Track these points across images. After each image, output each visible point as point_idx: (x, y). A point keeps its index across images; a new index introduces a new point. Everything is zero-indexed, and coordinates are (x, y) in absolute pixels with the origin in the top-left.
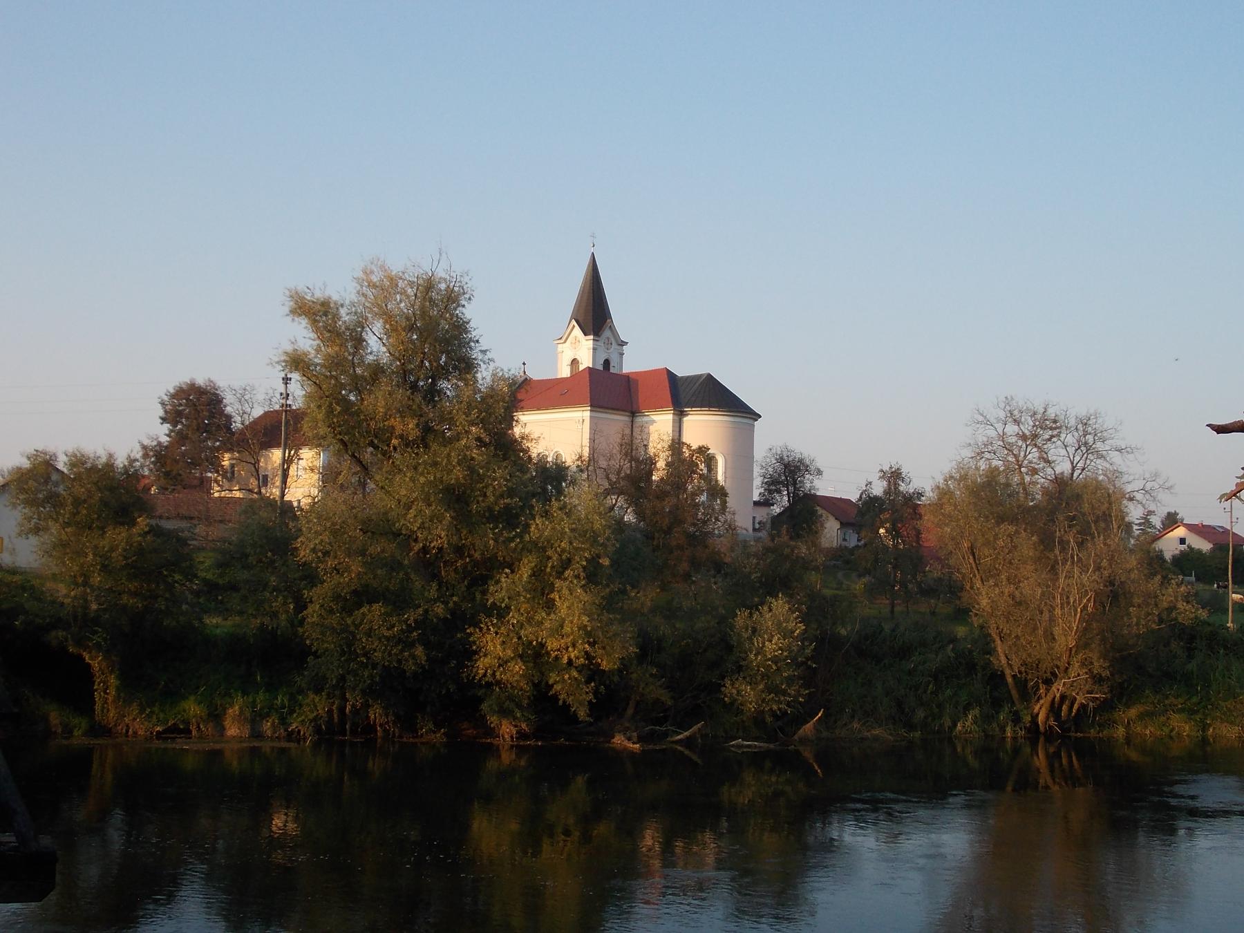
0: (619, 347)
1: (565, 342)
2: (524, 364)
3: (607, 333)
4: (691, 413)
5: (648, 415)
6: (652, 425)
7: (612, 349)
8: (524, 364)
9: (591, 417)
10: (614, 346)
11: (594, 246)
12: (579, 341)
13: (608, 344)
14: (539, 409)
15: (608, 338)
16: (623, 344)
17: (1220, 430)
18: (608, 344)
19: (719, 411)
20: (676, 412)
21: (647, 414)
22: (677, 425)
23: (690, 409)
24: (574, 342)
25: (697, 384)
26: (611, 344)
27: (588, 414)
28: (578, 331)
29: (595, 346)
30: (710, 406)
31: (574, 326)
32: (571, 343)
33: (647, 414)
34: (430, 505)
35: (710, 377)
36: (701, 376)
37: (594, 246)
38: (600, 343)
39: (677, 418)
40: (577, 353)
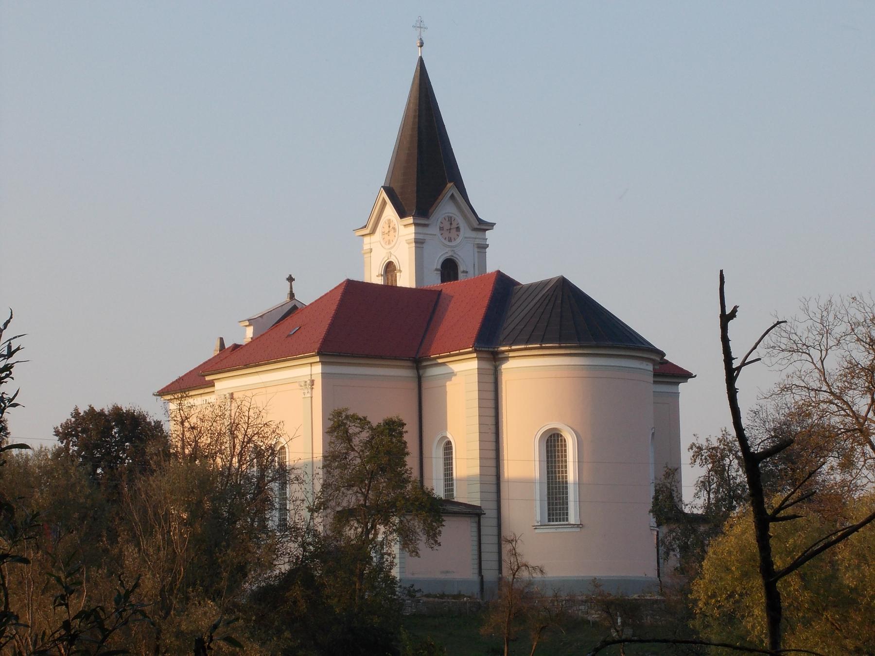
0: (474, 234)
1: (373, 232)
2: (291, 279)
3: (445, 209)
4: (511, 354)
5: (444, 364)
6: (450, 379)
7: (458, 240)
8: (291, 279)
9: (324, 375)
10: (465, 232)
11: (421, 46)
12: (394, 229)
13: (451, 229)
14: (247, 366)
15: (450, 220)
16: (484, 226)
17: (721, 271)
18: (451, 229)
19: (560, 348)
20: (485, 355)
21: (440, 361)
22: (491, 379)
23: (507, 348)
24: (387, 230)
25: (540, 295)
26: (458, 229)
27: (318, 369)
28: (390, 211)
29: (421, 237)
30: (543, 340)
31: (384, 200)
32: (383, 233)
33: (440, 361)
34: (859, 542)
35: (499, 272)
36: (547, 283)
37: (421, 46)
38: (434, 230)
39: (487, 366)
40: (392, 251)
